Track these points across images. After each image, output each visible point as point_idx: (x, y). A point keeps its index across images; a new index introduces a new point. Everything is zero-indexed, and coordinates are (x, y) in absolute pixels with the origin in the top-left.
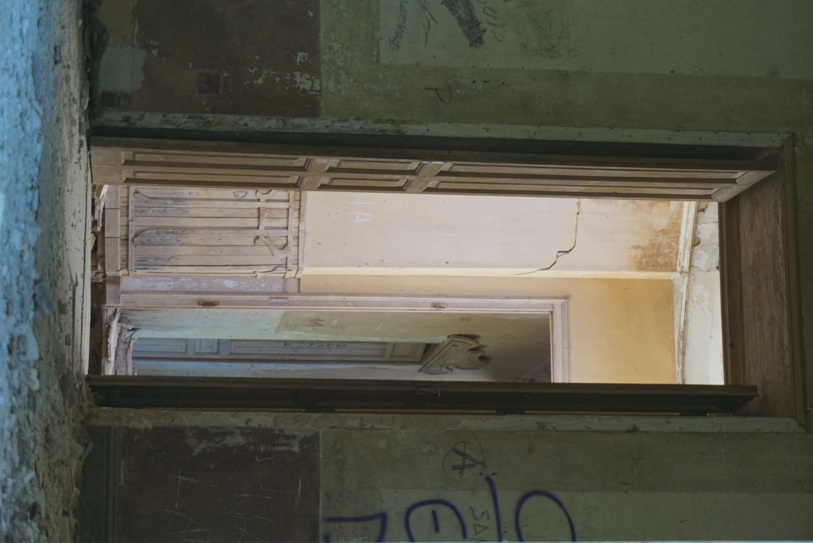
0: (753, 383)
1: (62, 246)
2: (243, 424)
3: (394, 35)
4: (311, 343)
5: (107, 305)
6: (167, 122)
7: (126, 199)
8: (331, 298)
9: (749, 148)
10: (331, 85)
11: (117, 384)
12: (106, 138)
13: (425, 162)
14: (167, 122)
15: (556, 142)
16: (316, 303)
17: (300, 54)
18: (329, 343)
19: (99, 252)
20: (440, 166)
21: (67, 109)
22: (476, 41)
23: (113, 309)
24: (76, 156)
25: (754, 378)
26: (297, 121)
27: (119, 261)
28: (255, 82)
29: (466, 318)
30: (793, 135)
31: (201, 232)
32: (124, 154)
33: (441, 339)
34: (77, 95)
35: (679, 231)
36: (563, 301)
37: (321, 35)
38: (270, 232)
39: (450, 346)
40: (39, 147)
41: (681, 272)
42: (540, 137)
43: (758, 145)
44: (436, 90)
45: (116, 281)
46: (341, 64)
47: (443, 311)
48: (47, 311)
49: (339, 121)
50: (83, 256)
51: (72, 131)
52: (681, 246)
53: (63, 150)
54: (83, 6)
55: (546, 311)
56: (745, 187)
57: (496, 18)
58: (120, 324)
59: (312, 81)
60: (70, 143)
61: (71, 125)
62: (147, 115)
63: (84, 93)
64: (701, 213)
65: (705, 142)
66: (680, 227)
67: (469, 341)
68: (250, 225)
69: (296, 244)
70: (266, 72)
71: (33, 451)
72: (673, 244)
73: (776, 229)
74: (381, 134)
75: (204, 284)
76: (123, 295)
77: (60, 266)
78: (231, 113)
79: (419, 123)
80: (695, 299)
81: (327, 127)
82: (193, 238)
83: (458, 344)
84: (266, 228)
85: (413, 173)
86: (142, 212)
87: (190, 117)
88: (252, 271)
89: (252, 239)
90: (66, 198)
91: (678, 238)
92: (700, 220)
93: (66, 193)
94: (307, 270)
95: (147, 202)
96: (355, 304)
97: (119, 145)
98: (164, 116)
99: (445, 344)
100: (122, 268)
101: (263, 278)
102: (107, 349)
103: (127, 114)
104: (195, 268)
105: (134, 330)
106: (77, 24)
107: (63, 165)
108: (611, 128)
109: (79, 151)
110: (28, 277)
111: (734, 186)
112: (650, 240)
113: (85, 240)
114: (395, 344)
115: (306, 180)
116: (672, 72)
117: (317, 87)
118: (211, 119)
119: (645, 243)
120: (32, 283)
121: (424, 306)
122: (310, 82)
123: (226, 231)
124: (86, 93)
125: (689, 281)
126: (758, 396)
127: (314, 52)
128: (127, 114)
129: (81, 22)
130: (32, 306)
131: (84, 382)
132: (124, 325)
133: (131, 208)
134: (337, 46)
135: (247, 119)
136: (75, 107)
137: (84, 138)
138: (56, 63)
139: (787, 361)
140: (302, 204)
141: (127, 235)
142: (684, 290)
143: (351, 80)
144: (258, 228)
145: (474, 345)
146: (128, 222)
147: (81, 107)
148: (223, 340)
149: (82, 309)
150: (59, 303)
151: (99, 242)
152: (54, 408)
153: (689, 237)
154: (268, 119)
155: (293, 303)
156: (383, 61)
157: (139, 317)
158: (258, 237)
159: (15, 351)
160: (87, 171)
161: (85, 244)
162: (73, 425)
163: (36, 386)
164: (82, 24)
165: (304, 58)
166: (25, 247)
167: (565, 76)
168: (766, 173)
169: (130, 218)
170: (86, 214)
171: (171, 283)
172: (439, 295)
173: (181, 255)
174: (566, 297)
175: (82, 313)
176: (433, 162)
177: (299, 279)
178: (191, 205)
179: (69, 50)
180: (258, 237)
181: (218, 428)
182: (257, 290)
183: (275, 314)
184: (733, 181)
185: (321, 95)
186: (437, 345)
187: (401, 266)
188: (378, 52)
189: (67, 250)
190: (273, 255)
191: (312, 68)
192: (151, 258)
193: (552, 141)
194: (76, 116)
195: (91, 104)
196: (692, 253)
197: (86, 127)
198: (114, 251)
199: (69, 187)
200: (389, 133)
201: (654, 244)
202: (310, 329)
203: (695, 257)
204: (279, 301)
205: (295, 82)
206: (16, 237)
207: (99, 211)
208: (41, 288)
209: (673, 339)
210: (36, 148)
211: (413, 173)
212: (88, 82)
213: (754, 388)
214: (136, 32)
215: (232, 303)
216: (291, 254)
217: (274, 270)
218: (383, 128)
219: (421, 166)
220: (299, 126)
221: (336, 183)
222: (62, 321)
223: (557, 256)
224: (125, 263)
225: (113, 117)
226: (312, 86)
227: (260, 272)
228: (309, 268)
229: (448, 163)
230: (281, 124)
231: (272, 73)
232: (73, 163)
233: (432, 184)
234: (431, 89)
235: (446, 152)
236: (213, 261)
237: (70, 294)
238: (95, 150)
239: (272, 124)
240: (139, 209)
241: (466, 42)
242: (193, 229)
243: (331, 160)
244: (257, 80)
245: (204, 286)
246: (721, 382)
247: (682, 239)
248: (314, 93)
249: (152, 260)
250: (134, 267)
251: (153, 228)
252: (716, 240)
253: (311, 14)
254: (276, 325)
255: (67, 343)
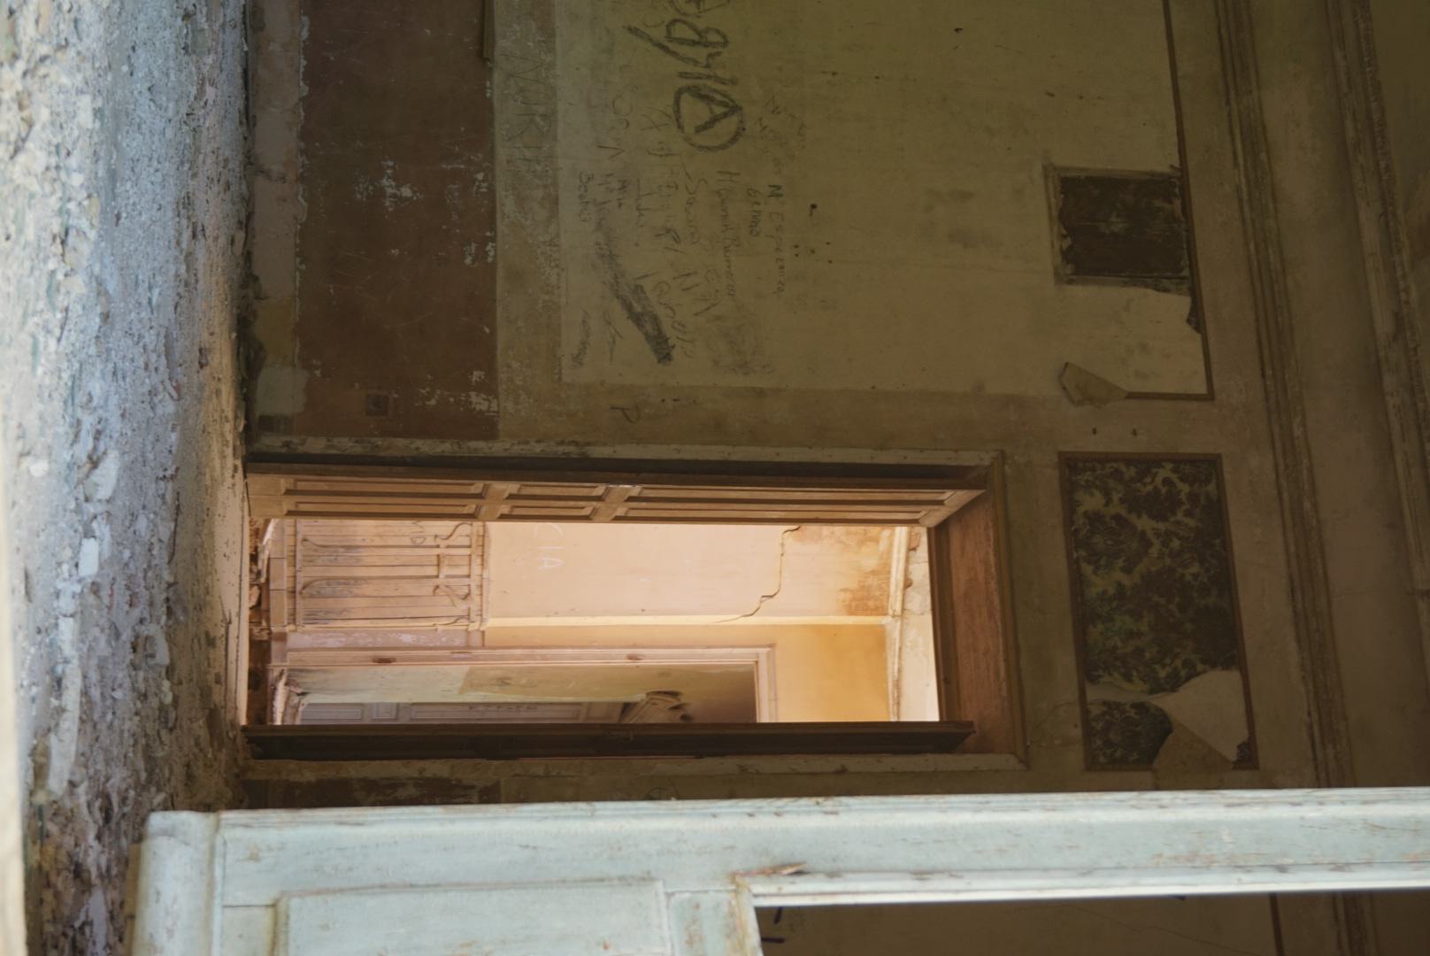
0: (970, 719)
1: (211, 573)
2: (416, 775)
3: (576, 352)
4: (499, 705)
5: (273, 664)
6: (332, 447)
7: (292, 548)
8: (518, 652)
9: (957, 467)
10: (510, 406)
11: (276, 734)
12: (264, 465)
13: (611, 486)
14: (332, 447)
15: (750, 464)
16: (502, 658)
17: (476, 373)
18: (518, 705)
19: (264, 606)
20: (628, 490)
21: (217, 427)
22: (665, 358)
23: (279, 669)
24: (229, 481)
25: (970, 713)
26: (473, 444)
27: (286, 615)
28: (428, 403)
29: (665, 673)
30: (1003, 452)
31: (375, 581)
32: (284, 482)
33: (639, 697)
34: (230, 415)
35: (889, 572)
36: (768, 649)
37: (499, 352)
38: (451, 580)
39: (649, 705)
40: (174, 437)
41: (894, 616)
42: (735, 458)
43: (966, 464)
44: (623, 410)
45: (282, 637)
46: (520, 383)
47: (640, 663)
48: (182, 618)
49: (519, 443)
50: (238, 592)
51: (223, 451)
52: (893, 588)
53: (213, 469)
54: (238, 321)
55: (750, 661)
56: (954, 509)
57: (685, 333)
58: (288, 688)
59: (490, 402)
60: (221, 464)
61: (223, 445)
62: (310, 440)
63: (239, 414)
64: (912, 552)
65: (909, 461)
66: (890, 567)
67: (669, 699)
68: (428, 573)
69: (479, 593)
70: (439, 392)
71: (169, 780)
72: (884, 585)
73: (987, 553)
74: (563, 456)
75: (379, 639)
76: (290, 653)
77: (208, 593)
78: (402, 437)
79: (605, 444)
80: (909, 644)
81: (506, 450)
82: (368, 589)
83: (658, 702)
84: (448, 577)
85: (599, 499)
86: (310, 561)
87: (357, 442)
88: (431, 624)
89: (431, 589)
90: (216, 523)
91: (888, 579)
92: (912, 559)
93: (217, 517)
94: (492, 622)
95: (315, 550)
96: (544, 658)
97: (278, 472)
98: (329, 441)
99: (644, 703)
100: (289, 624)
101: (444, 631)
102: (272, 713)
103: (288, 439)
104: (369, 621)
105: (303, 694)
106: (230, 338)
107: (213, 485)
108: (810, 448)
109: (233, 477)
110: (158, 577)
111: (942, 508)
112: (860, 582)
113: (240, 576)
114: (590, 704)
115: (484, 509)
116: (873, 388)
117: (494, 407)
118: (380, 443)
119: (853, 585)
120: (164, 586)
121: (619, 659)
122: (486, 403)
123: (404, 581)
124: (241, 415)
125: (902, 626)
126: (974, 732)
127: (491, 370)
128: (288, 439)
129: (234, 335)
130: (164, 609)
131: (240, 732)
132: (293, 689)
133: (299, 556)
134: (515, 365)
135: (419, 443)
136: (228, 427)
137: (239, 463)
138: (202, 366)
139: (1004, 693)
140: (486, 550)
141: (295, 587)
142: (896, 634)
143: (531, 401)
144: (437, 577)
145: (675, 702)
146: (296, 572)
147: (236, 428)
148: (403, 704)
149: (238, 651)
150: (207, 634)
151: (264, 595)
152: (197, 744)
153: (900, 577)
154: (442, 442)
155: (476, 658)
156: (566, 379)
157: (308, 679)
158: (437, 587)
159: (140, 650)
160: (243, 500)
161: (241, 580)
162: (225, 775)
163: (168, 699)
164: (237, 337)
165: (480, 378)
166: (154, 540)
167: (760, 393)
168: (975, 493)
169: (298, 566)
170: (242, 548)
171: (343, 639)
172: (635, 646)
173: (353, 608)
174: (771, 646)
175: (237, 656)
176: (621, 486)
177: (483, 632)
178: (364, 552)
179: (221, 363)
180: (437, 587)
181: (388, 779)
182: (438, 644)
183: (459, 670)
184: (941, 503)
185: (499, 416)
186: (635, 704)
187: (593, 614)
188: (560, 371)
189: (218, 580)
190: (454, 605)
191: (489, 388)
192: (321, 611)
193: (749, 463)
194: (230, 437)
195: (247, 428)
196: (904, 595)
197: (241, 451)
198: (280, 605)
199: (220, 511)
200: (573, 456)
201: (863, 587)
202: (496, 688)
203: (908, 599)
204: (462, 656)
205: (471, 403)
206: (142, 524)
207: (263, 561)
208: (175, 591)
209: (887, 689)
210: (170, 437)
211: (599, 499)
212: (244, 403)
213: (971, 724)
214: (297, 350)
215: (411, 659)
216: (474, 605)
217: (455, 622)
218: (567, 451)
219: (608, 491)
220: (476, 450)
221: (517, 512)
222: (211, 656)
223: (761, 602)
224: (292, 617)
225: (271, 442)
226: (489, 407)
227: (441, 625)
228: (495, 619)
229: (637, 486)
230: (456, 447)
231: (446, 393)
232: (226, 487)
233: (620, 512)
234: (617, 408)
235: (634, 475)
236: (388, 613)
237: (223, 631)
238: (252, 478)
239: (445, 448)
240: (308, 559)
241: (653, 358)
242: (366, 579)
243: (511, 485)
244: (429, 400)
245: (380, 641)
246: (932, 715)
247: (893, 580)
248: (492, 414)
249: (322, 614)
250: (302, 622)
251: (323, 578)
252: (927, 581)
253: (487, 330)
254: (459, 685)
255: (218, 682)
